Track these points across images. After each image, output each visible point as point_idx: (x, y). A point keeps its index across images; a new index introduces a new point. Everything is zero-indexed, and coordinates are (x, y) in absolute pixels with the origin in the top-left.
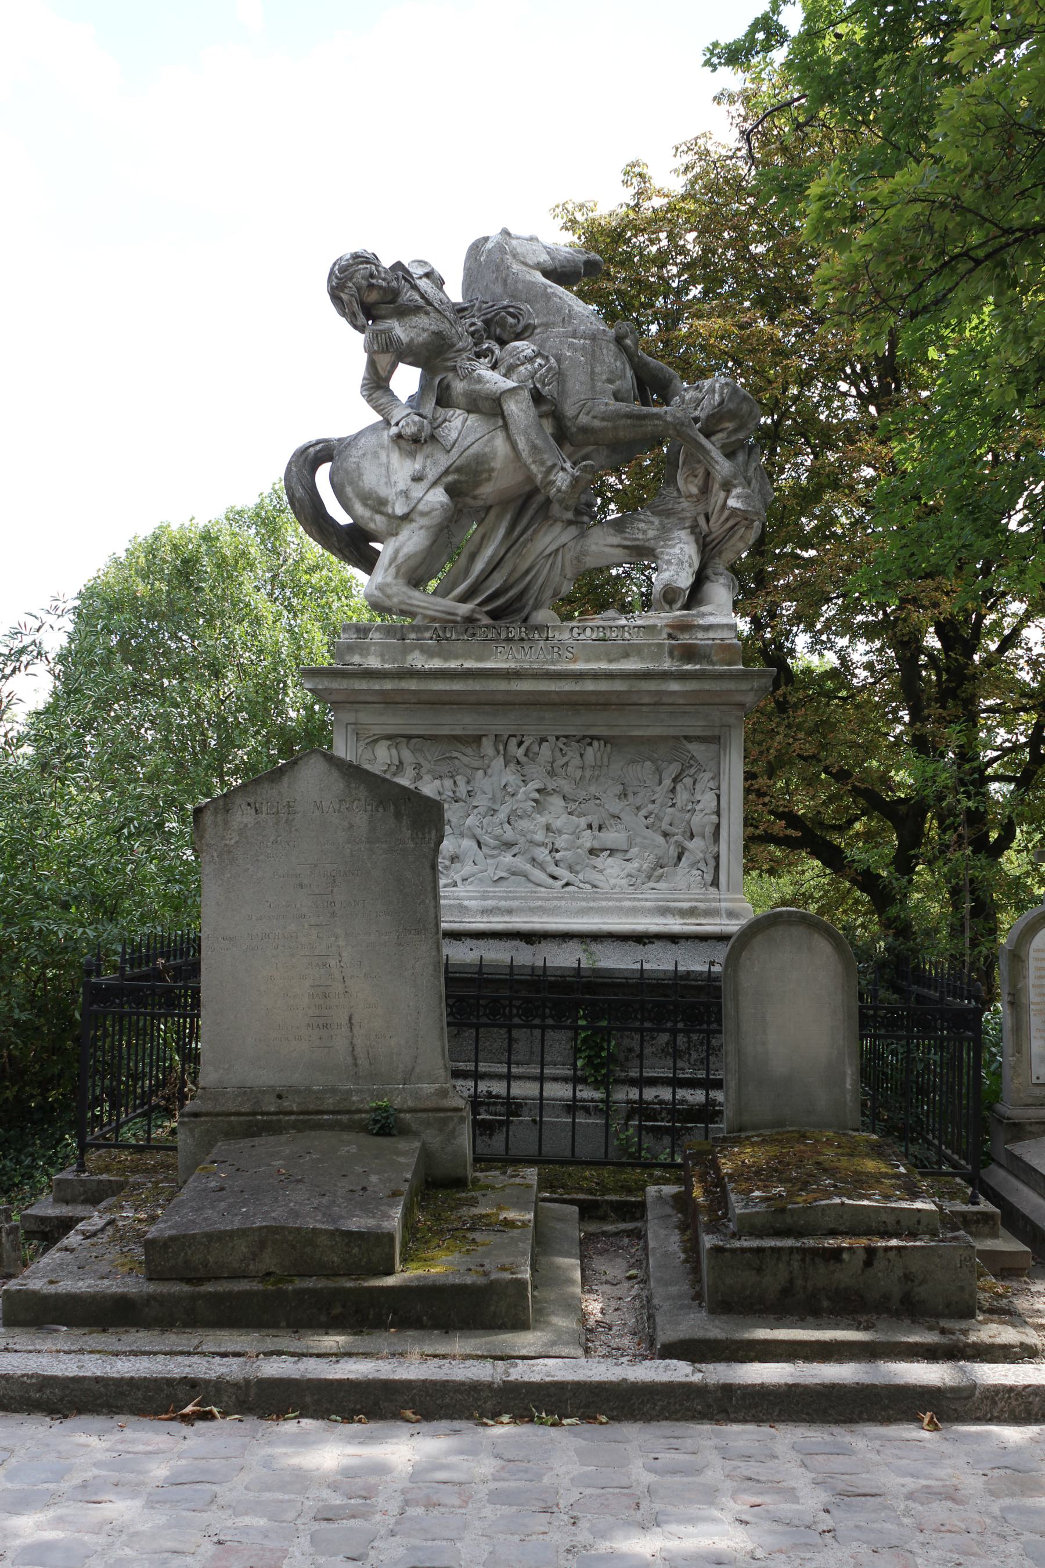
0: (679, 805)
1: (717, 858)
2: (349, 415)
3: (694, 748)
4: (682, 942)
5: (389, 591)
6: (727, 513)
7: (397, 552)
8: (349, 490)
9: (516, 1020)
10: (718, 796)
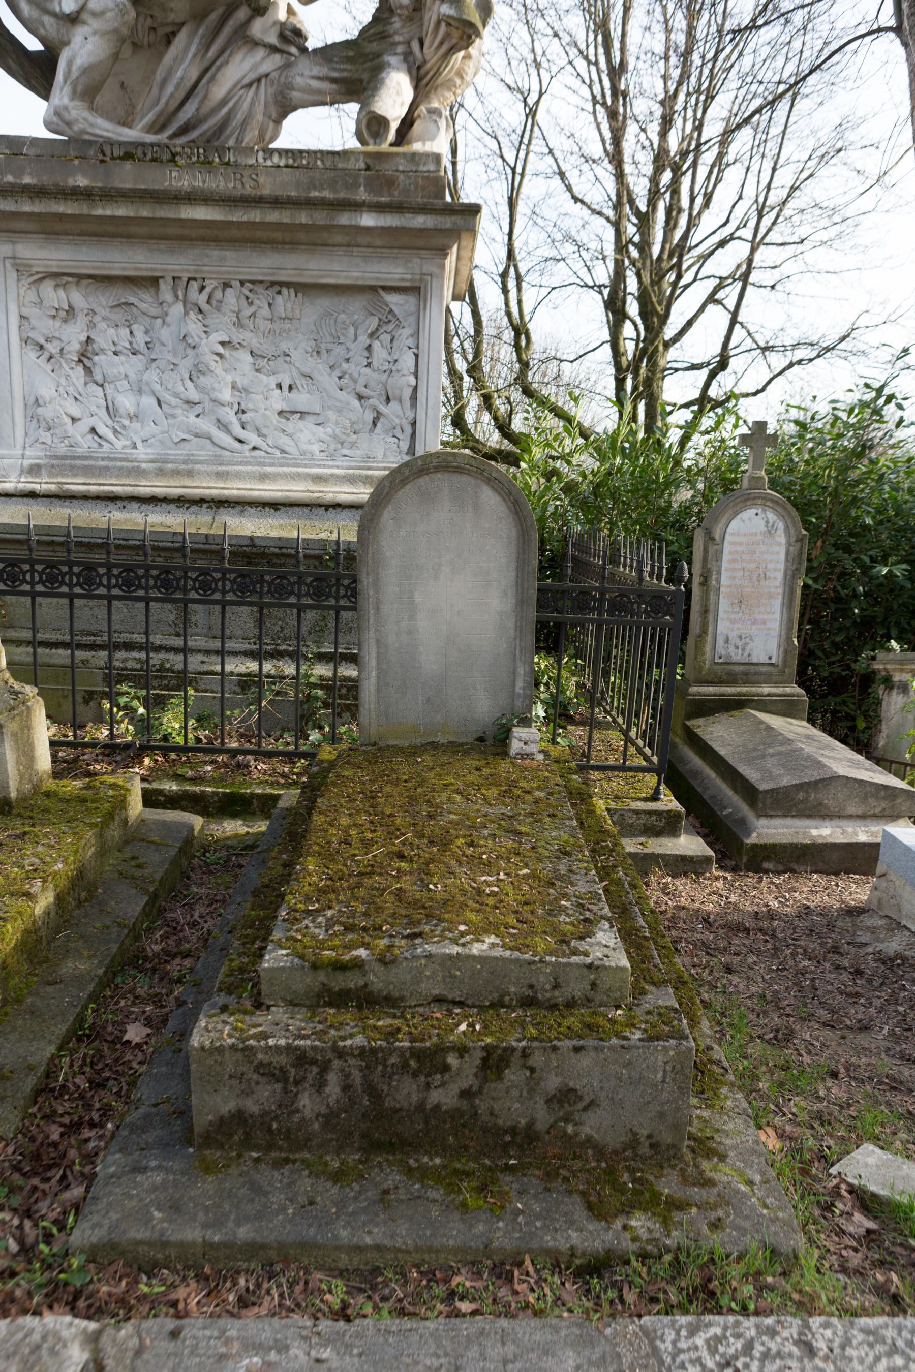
0: (375, 364)
1: (414, 424)
3: (393, 299)
5: (67, 117)
9: (193, 595)
10: (417, 356)
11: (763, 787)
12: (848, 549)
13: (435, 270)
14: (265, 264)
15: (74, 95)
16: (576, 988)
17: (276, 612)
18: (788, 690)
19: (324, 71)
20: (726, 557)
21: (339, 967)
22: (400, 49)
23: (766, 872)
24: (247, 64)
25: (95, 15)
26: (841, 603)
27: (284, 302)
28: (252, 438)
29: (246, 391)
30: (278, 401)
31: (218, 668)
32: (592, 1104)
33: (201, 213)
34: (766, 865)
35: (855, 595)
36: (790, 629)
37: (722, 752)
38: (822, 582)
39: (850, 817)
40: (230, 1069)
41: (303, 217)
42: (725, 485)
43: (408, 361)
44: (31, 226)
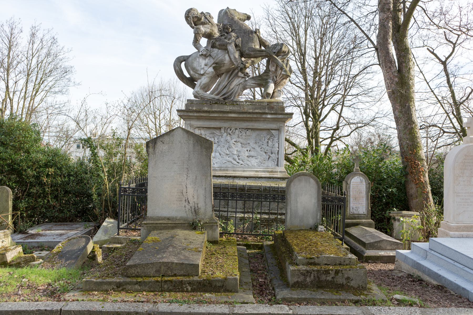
0: (269, 145)
1: (278, 159)
2: (190, 50)
3: (273, 131)
4: (275, 179)
6: (281, 75)
7: (201, 83)
8: (189, 68)
11: (367, 242)
12: (380, 184)
13: (283, 126)
14: (245, 125)
15: (201, 89)
16: (347, 262)
17: (247, 202)
18: (369, 221)
19: (254, 82)
20: (351, 188)
21: (311, 258)
22: (271, 78)
23: (370, 263)
24: (237, 81)
25: (207, 74)
26: (380, 199)
27: (248, 132)
28: (241, 162)
29: (240, 151)
30: (247, 153)
31: (235, 216)
32: (352, 280)
33: (233, 115)
34: (369, 261)
35: (383, 196)
36: (368, 205)
37: (355, 235)
38: (374, 193)
39: (388, 250)
40: (297, 273)
41: (255, 116)
42: (347, 170)
43: (277, 145)
44: (194, 118)
